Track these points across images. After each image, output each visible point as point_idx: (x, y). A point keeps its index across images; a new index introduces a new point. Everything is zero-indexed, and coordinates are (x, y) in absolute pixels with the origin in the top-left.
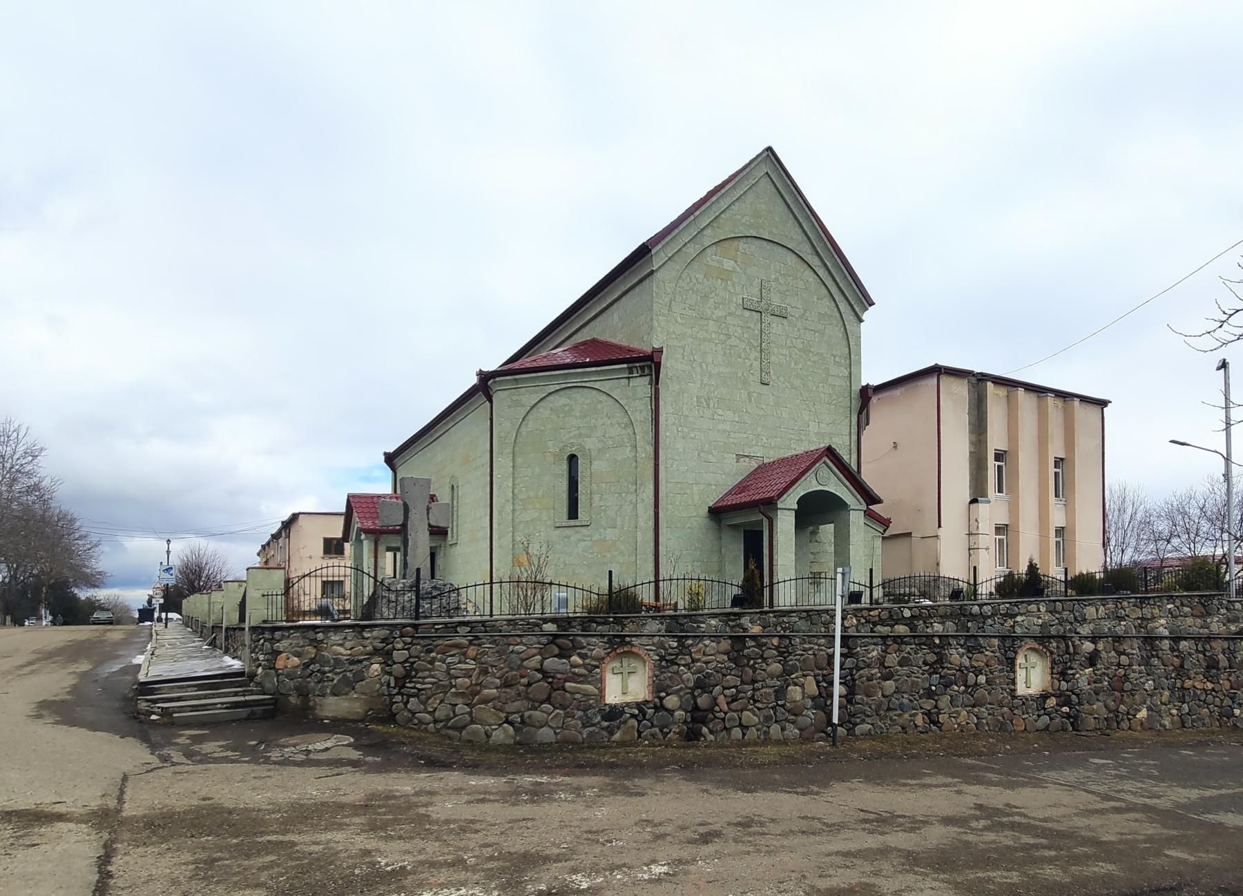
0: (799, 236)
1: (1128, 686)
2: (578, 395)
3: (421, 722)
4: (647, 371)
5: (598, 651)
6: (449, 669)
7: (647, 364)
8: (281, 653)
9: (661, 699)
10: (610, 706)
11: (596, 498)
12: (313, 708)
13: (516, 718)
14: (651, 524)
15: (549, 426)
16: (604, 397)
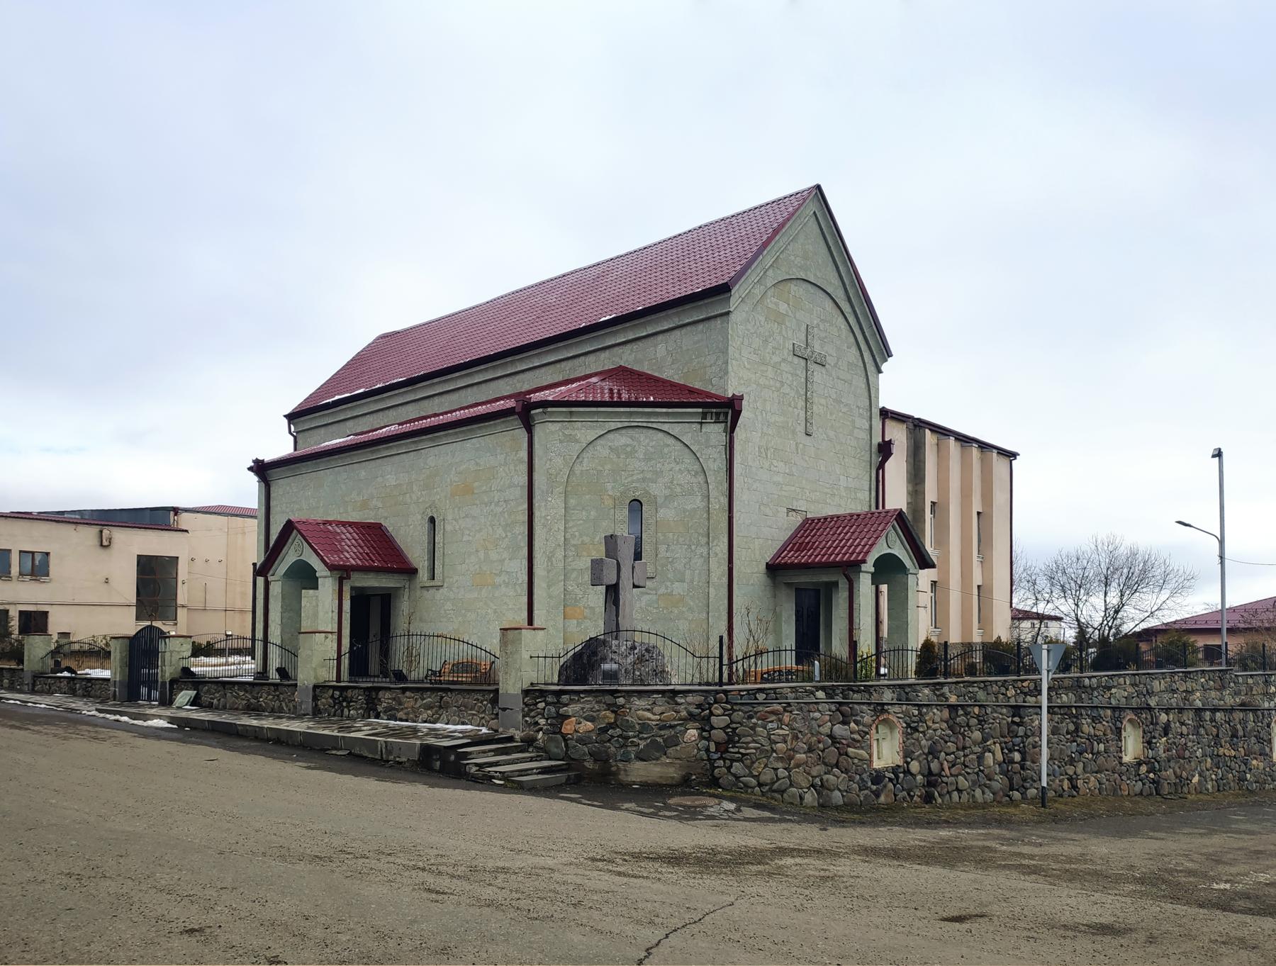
0: (837, 282)
1: (1187, 754)
2: (642, 436)
3: (746, 785)
4: (722, 418)
5: (867, 719)
6: (769, 735)
7: (727, 410)
8: (569, 717)
9: (908, 763)
10: (876, 771)
11: (662, 548)
12: (616, 774)
13: (817, 781)
14: (725, 580)
15: (608, 467)
16: (671, 441)
